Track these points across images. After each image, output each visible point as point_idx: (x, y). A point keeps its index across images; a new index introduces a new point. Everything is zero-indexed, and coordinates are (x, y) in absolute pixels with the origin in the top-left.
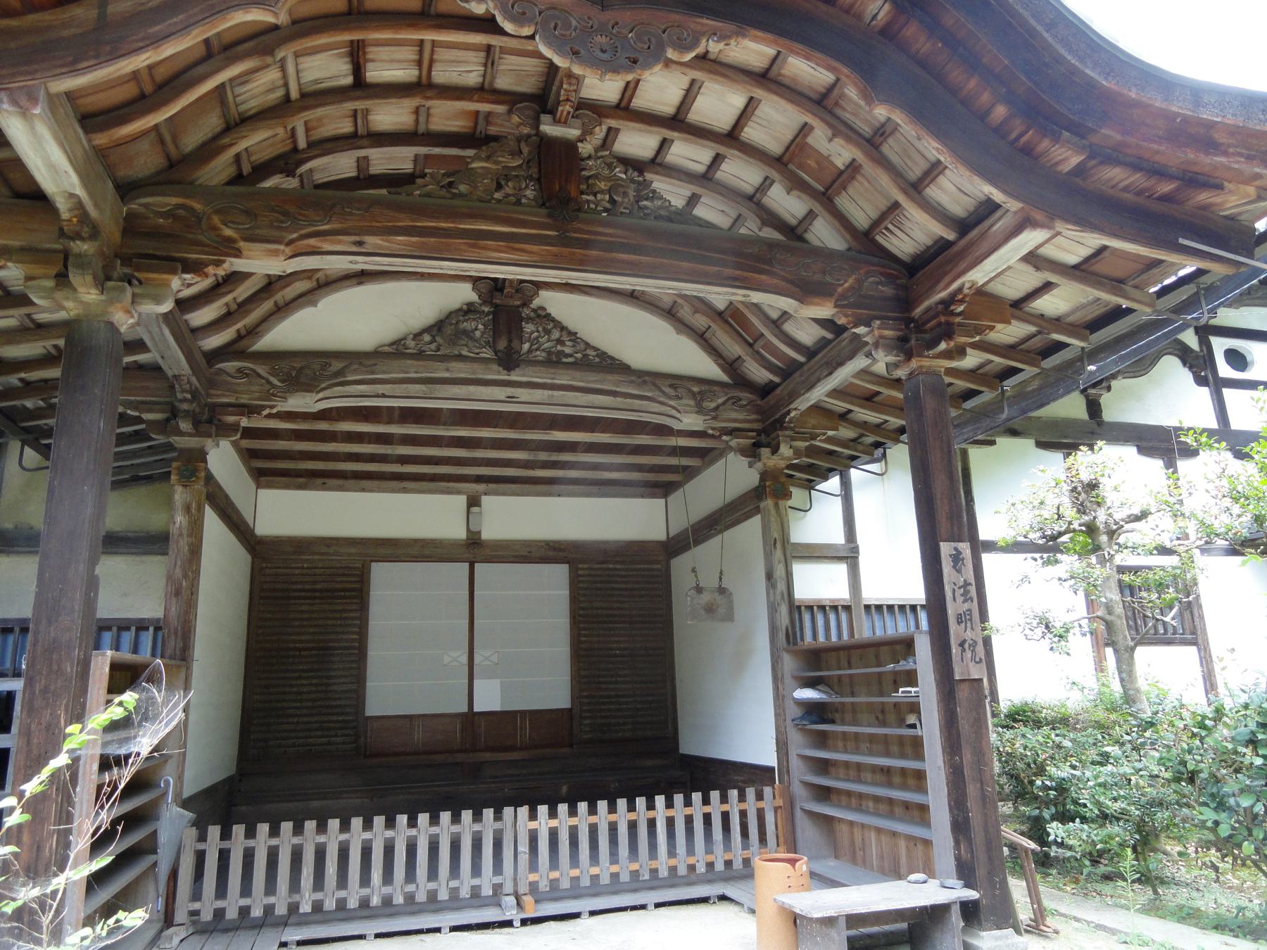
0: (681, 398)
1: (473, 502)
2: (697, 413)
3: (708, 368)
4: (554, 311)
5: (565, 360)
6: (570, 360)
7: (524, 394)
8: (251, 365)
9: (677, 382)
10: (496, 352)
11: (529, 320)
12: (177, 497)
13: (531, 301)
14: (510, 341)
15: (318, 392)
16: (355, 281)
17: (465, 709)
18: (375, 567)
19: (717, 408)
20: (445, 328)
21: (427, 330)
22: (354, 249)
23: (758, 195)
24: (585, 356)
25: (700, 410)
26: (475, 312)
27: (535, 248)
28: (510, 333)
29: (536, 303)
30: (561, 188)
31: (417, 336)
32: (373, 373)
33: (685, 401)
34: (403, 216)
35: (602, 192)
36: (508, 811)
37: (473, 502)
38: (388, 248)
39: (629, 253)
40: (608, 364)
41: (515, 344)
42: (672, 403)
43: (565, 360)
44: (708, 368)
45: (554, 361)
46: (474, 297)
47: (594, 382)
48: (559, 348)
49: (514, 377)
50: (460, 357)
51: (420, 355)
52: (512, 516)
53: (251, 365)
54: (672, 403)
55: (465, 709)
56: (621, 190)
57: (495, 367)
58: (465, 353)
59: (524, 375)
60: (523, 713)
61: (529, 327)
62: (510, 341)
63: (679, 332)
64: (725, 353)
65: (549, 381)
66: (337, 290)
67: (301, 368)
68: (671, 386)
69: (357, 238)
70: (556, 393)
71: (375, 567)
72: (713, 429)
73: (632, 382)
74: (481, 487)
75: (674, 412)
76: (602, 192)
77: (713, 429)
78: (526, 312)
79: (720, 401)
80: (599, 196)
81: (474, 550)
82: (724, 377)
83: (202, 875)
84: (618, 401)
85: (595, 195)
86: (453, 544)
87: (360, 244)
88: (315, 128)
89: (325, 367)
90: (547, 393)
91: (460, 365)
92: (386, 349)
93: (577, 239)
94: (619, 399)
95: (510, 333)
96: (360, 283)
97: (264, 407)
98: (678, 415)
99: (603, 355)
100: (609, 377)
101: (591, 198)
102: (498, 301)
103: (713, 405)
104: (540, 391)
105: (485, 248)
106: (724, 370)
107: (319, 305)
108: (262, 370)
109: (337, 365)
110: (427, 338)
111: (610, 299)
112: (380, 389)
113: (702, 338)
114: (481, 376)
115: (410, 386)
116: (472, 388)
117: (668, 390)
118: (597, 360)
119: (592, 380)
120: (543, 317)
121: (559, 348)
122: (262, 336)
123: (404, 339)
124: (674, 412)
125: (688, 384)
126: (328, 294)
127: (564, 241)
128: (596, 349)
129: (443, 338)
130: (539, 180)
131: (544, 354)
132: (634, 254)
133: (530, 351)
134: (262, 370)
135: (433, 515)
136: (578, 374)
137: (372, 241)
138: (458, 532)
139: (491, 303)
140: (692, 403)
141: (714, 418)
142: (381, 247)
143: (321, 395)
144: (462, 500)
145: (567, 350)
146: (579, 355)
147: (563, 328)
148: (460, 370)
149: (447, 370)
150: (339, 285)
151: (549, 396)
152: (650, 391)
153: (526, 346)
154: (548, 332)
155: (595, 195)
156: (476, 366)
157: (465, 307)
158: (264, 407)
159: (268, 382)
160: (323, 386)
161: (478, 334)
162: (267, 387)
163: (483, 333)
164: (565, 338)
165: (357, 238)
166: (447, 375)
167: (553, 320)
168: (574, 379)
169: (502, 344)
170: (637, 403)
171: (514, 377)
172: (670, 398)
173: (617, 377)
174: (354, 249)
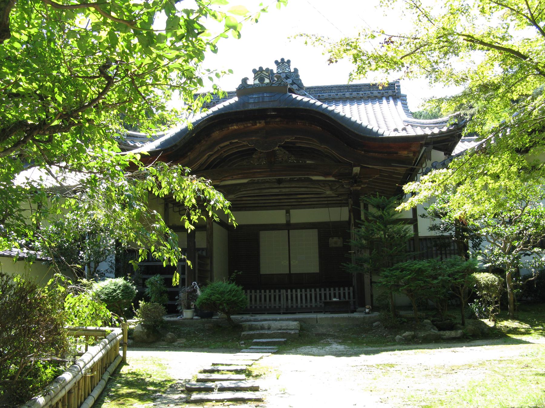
1: (288, 212)
12: (220, 197)
17: (288, 272)
18: (196, 247)
25: (331, 189)
36: (282, 291)
37: (288, 212)
49: (281, 186)
52: (299, 216)
55: (288, 272)
60: (305, 274)
71: (196, 247)
74: (289, 207)
81: (288, 226)
83: (258, 399)
84: (309, 189)
86: (282, 225)
135: (277, 217)
137: (235, 177)
138: (283, 221)
144: (284, 211)
171: (281, 186)
172: (322, 186)
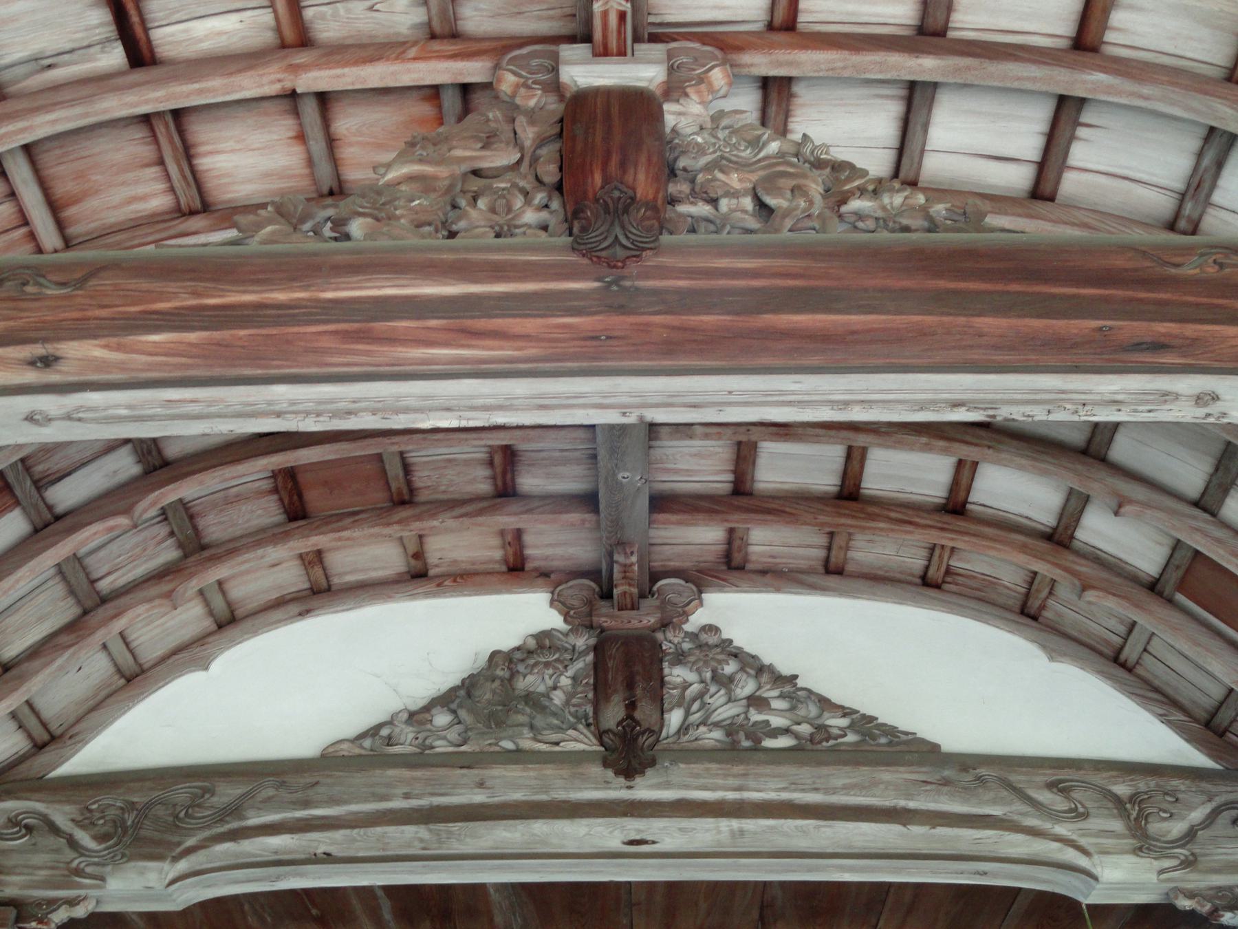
0: (1085, 816)
2: (1137, 851)
3: (1146, 737)
4: (741, 636)
5: (769, 743)
6: (783, 742)
7: (669, 834)
8: (40, 807)
9: (1067, 779)
10: (600, 736)
11: (680, 658)
13: (685, 615)
14: (631, 706)
15: (176, 859)
16: (294, 608)
19: (1190, 835)
20: (491, 694)
21: (445, 700)
22: (31, 376)
23: (1188, 208)
24: (821, 728)
26: (552, 648)
27: (530, 325)
28: (630, 686)
29: (698, 619)
30: (606, 180)
31: (418, 717)
32: (306, 804)
33: (1094, 823)
34: (172, 287)
35: (735, 194)
38: (122, 367)
39: (815, 310)
40: (881, 745)
41: (645, 712)
42: (1061, 830)
43: (769, 743)
44: (1146, 737)
45: (742, 746)
46: (553, 620)
47: (846, 788)
48: (756, 716)
50: (518, 756)
51: (421, 759)
53: (40, 807)
54: (1061, 830)
56: (788, 183)
57: (596, 770)
58: (527, 744)
59: (667, 785)
61: (677, 674)
62: (631, 706)
63: (1053, 654)
64: (1185, 694)
65: (731, 796)
66: (255, 632)
67: (149, 806)
68: (1051, 786)
69: (39, 350)
70: (750, 824)
72: (1191, 895)
73: (946, 782)
75: (1071, 856)
76: (735, 194)
77: (1191, 895)
78: (670, 641)
79: (1197, 815)
80: (724, 204)
82: (1197, 758)
84: (916, 836)
85: (714, 202)
87: (47, 362)
88: (76, 200)
89: (195, 803)
90: (727, 825)
91: (513, 772)
92: (346, 749)
93: (655, 292)
94: (916, 829)
95: (630, 686)
96: (303, 614)
97: (53, 904)
98: (1083, 861)
99: (864, 724)
100: (886, 775)
101: (703, 209)
102: (607, 622)
103: (1177, 828)
104: (708, 823)
105: (392, 340)
106: (1191, 738)
107: (216, 666)
108: (61, 815)
109: (227, 793)
110: (442, 719)
111: (873, 596)
112: (322, 841)
113: (1118, 662)
114: (561, 795)
115: (391, 830)
116: (540, 827)
117: (1045, 797)
118: (851, 738)
119: (841, 784)
120: (715, 649)
121: (756, 716)
122: (85, 742)
123: (390, 723)
124: (1071, 856)
125: (1099, 779)
126: (234, 642)
127: (617, 302)
128: (846, 712)
129: (471, 711)
130: (559, 187)
131: (717, 734)
132: (829, 310)
133: (684, 728)
134: (61, 815)
136: (805, 773)
137: (80, 353)
139: (591, 627)
140: (1117, 825)
141: (1189, 863)
142: (102, 366)
143: (183, 866)
145: (777, 721)
146: (805, 729)
147: (760, 669)
148: (512, 783)
149: (481, 785)
150: (261, 619)
151: (725, 837)
152: (994, 802)
153: (675, 718)
154: (726, 682)
155: (714, 202)
156: (549, 770)
157: (532, 643)
158: (53, 904)
159: (72, 843)
160: (190, 842)
161: (558, 698)
162: (69, 854)
163: (570, 696)
164: (770, 693)
165: (39, 350)
166: (479, 797)
167: (737, 654)
168: (794, 786)
169: (613, 714)
170: (966, 838)
171: (645, 790)
172: (1056, 816)
173: (901, 775)
174: (31, 376)
